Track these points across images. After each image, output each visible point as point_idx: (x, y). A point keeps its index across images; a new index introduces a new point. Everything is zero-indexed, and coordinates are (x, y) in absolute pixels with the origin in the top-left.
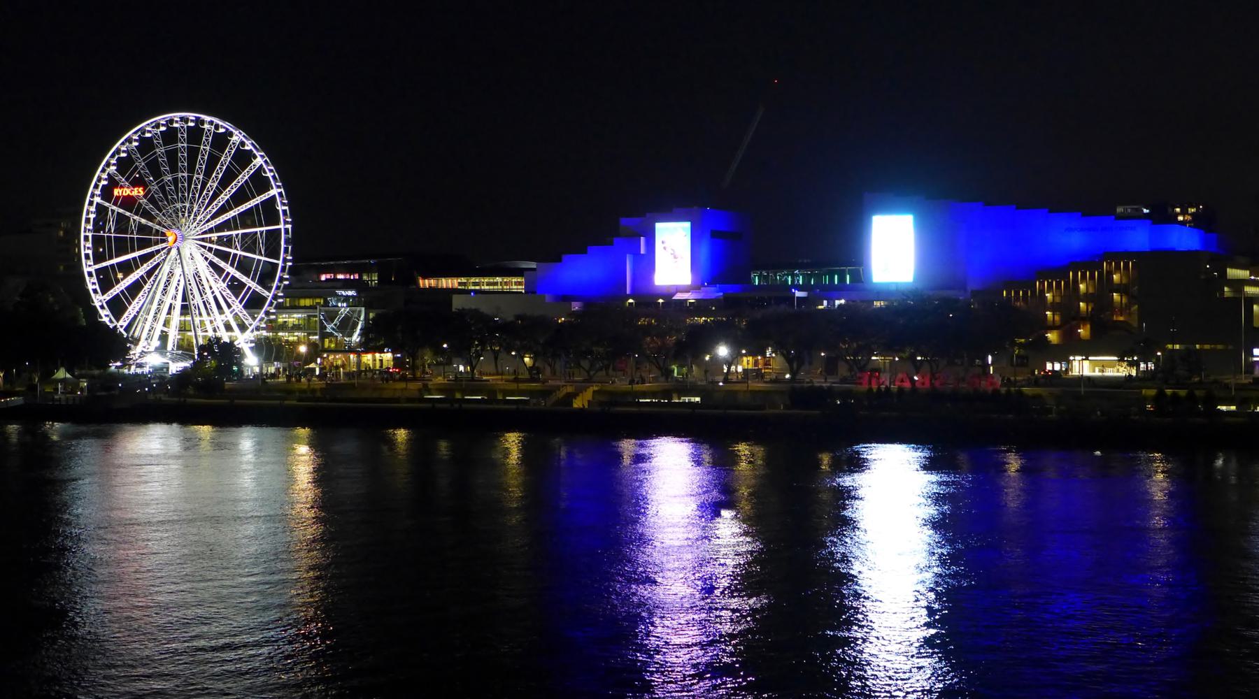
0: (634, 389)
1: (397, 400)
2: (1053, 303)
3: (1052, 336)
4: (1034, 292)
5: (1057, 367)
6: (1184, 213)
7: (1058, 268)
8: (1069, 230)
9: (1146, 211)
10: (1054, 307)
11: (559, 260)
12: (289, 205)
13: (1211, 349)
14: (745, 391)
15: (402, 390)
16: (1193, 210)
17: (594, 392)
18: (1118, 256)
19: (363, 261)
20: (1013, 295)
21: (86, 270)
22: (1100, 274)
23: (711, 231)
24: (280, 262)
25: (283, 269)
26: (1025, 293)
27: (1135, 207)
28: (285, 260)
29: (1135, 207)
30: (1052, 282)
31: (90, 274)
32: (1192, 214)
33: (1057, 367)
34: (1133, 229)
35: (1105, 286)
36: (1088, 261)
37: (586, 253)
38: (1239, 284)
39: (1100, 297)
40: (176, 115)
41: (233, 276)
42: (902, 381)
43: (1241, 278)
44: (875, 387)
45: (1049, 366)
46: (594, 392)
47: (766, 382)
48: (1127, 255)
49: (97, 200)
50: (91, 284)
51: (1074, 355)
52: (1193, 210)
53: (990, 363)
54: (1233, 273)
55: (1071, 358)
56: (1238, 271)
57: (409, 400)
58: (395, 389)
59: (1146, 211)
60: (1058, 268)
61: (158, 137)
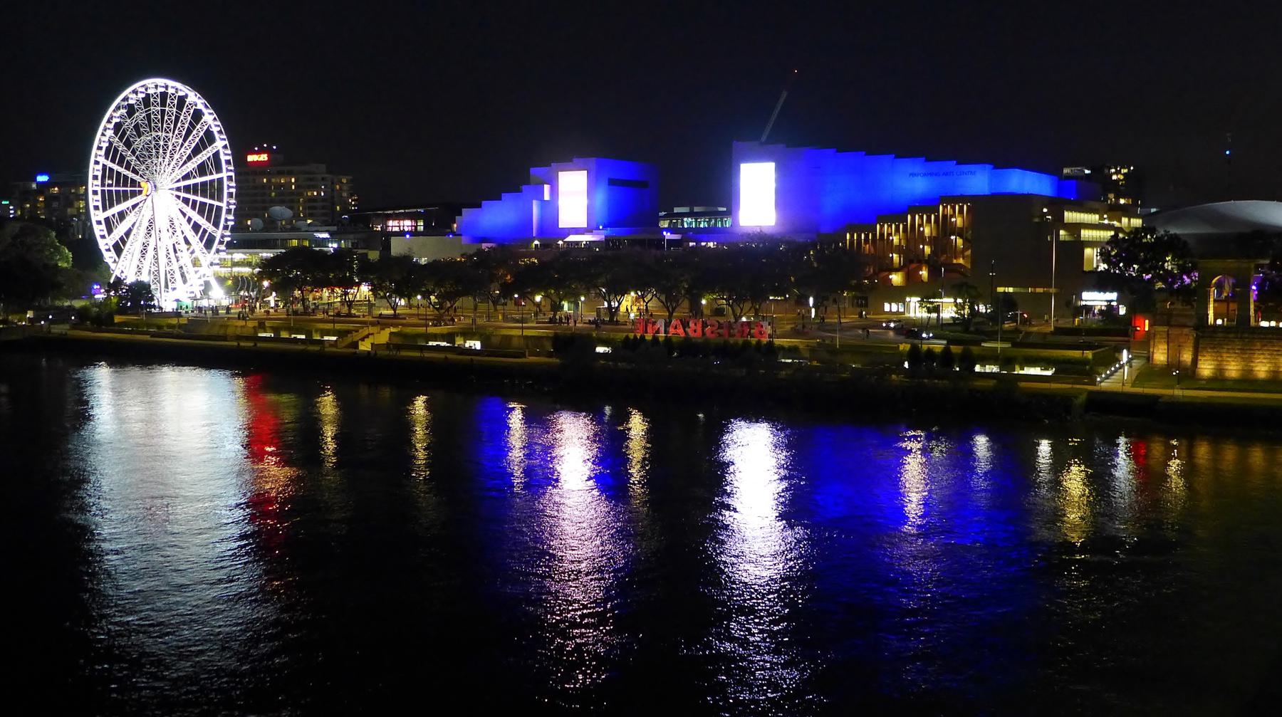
0: (428, 331)
1: (224, 338)
2: (900, 246)
3: (896, 278)
4: (874, 235)
5: (894, 307)
6: (1117, 173)
7: (896, 213)
8: (913, 175)
9: (1087, 172)
10: (899, 250)
11: (479, 206)
12: (233, 154)
13: (1044, 293)
14: (519, 336)
15: (242, 327)
16: (1126, 171)
17: (391, 333)
18: (953, 199)
19: (409, 211)
20: (855, 238)
21: (94, 219)
22: (937, 218)
23: (609, 179)
24: (224, 205)
25: (229, 211)
26: (867, 236)
27: (1079, 168)
28: (229, 204)
29: (1079, 168)
30: (899, 225)
31: (99, 223)
32: (1124, 174)
33: (894, 307)
34: (973, 173)
35: (945, 228)
36: (927, 205)
37: (500, 199)
38: (1076, 228)
39: (940, 241)
40: (171, 83)
41: (195, 222)
42: (676, 328)
43: (1078, 222)
44: (649, 337)
45: (887, 307)
46: (391, 333)
47: (585, 323)
48: (962, 199)
49: (102, 160)
50: (99, 230)
51: (911, 296)
52: (1126, 171)
53: (811, 305)
54: (1070, 216)
55: (908, 299)
56: (1082, 214)
57: (239, 338)
58: (236, 326)
59: (1087, 172)
60: (896, 213)
61: (140, 102)
